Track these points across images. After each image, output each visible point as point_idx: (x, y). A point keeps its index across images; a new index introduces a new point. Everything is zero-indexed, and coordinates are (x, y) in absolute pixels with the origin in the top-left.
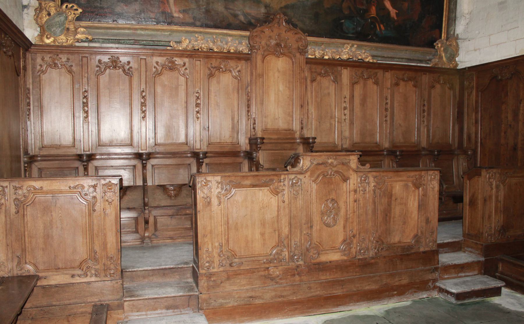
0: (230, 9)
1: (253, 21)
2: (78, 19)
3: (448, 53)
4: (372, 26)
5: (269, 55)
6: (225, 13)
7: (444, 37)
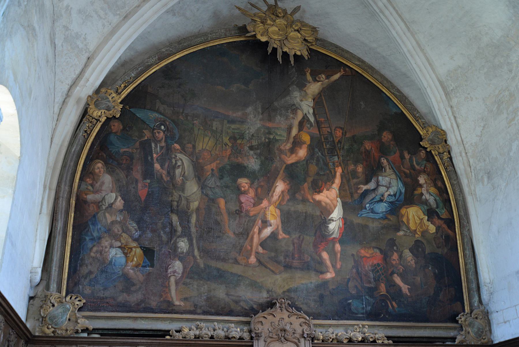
0: (232, 295)
1: (255, 306)
2: (80, 309)
3: (476, 327)
4: (383, 304)
5: (272, 341)
6: (227, 299)
7: (468, 309)
